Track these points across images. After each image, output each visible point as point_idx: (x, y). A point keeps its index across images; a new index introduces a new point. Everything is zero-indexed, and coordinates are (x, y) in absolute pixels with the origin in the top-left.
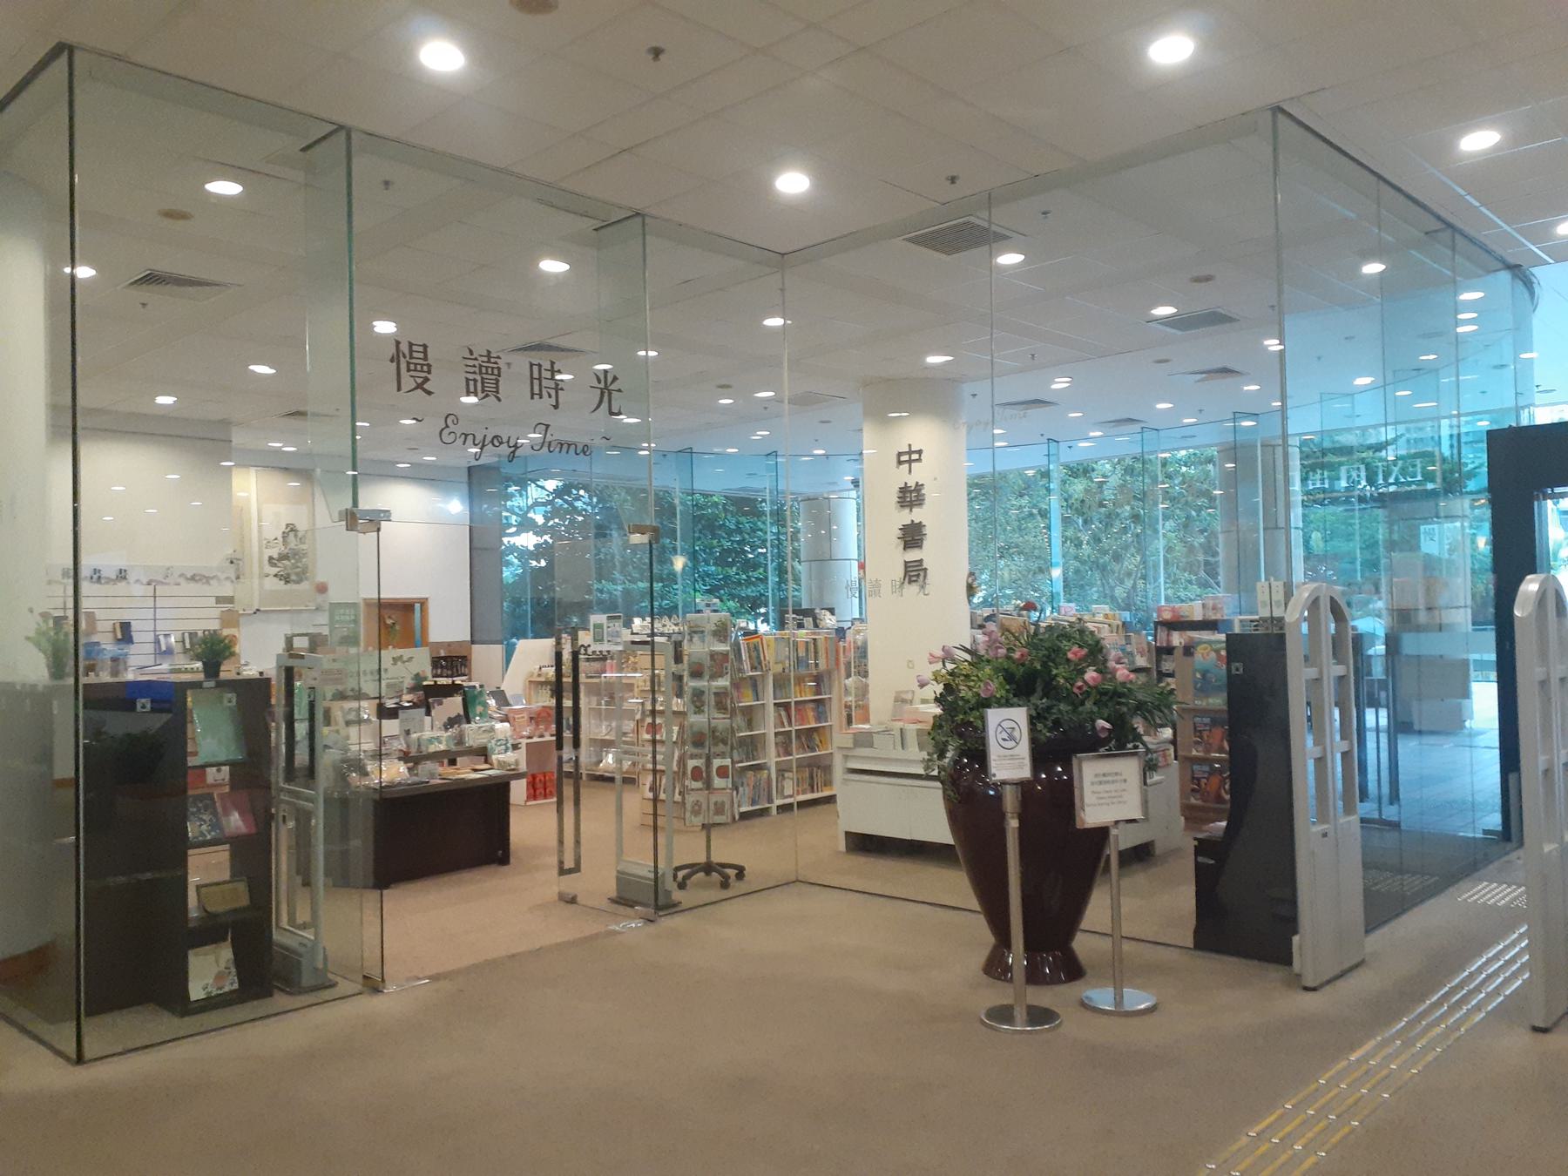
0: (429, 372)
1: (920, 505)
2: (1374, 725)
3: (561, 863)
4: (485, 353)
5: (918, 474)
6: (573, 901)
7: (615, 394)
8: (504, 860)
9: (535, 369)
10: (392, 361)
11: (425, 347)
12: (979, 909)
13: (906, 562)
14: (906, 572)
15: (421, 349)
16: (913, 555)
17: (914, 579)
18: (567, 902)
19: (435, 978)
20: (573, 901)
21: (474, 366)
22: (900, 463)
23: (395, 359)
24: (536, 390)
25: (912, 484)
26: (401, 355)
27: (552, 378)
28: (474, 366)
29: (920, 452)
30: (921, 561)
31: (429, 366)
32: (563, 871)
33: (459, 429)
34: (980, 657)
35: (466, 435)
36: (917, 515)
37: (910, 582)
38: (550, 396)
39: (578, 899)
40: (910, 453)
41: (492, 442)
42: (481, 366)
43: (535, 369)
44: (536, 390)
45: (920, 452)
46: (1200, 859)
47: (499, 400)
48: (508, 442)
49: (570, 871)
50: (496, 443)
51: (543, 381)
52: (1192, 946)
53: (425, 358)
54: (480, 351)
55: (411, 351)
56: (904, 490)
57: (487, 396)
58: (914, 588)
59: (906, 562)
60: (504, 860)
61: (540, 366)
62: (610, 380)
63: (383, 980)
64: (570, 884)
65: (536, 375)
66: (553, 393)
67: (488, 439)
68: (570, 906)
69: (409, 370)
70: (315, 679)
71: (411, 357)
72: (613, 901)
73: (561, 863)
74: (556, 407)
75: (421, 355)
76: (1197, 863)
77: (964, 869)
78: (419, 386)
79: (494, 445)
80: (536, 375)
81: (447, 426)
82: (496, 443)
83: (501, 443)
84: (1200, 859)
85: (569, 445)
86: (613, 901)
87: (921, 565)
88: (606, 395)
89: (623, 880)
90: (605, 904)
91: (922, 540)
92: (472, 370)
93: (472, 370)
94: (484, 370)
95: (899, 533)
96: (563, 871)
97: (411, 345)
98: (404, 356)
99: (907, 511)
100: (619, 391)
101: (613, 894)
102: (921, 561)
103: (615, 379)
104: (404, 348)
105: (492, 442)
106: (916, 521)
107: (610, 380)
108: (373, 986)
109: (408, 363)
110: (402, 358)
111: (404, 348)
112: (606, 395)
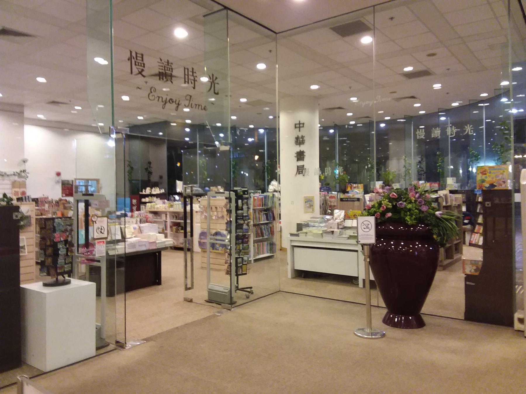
0: (144, 67)
1: (303, 144)
2: (114, 232)
3: (186, 285)
4: (167, 61)
5: (303, 132)
6: (191, 301)
7: (216, 85)
8: (159, 283)
9: (186, 70)
10: (129, 60)
11: (142, 55)
12: (385, 307)
13: (298, 166)
14: (298, 169)
15: (141, 56)
16: (300, 163)
17: (301, 172)
18: (189, 302)
19: (147, 340)
20: (191, 301)
21: (162, 66)
22: (296, 127)
23: (130, 59)
24: (187, 80)
25: (300, 136)
26: (132, 57)
27: (193, 75)
28: (162, 66)
29: (303, 124)
30: (303, 166)
31: (144, 64)
32: (187, 289)
33: (156, 95)
34: (202, 212)
35: (159, 97)
36: (302, 148)
37: (299, 173)
38: (192, 83)
39: (193, 300)
40: (300, 124)
41: (169, 101)
42: (165, 67)
43: (186, 70)
44: (187, 80)
45: (303, 124)
46: (468, 283)
47: (172, 82)
48: (176, 102)
49: (190, 289)
50: (171, 101)
51: (189, 76)
52: (463, 318)
53: (142, 60)
54: (165, 59)
55: (136, 56)
56: (297, 138)
57: (167, 80)
58: (301, 175)
59: (298, 166)
60: (159, 283)
61: (188, 69)
62: (214, 78)
63: (126, 343)
64: (190, 294)
65: (186, 73)
66: (193, 82)
67: (168, 99)
68: (190, 303)
69: (136, 65)
70: (96, 205)
71: (137, 59)
72: (207, 301)
73: (186, 285)
74: (194, 88)
75: (141, 59)
76: (466, 284)
77: (378, 288)
78: (140, 73)
79: (170, 103)
80: (186, 73)
81: (151, 92)
82: (171, 101)
83: (173, 102)
84: (468, 283)
85: (199, 105)
86: (207, 301)
87: (303, 167)
88: (213, 84)
89: (211, 292)
90: (203, 302)
91: (304, 158)
92: (161, 68)
93: (161, 68)
94: (166, 69)
95: (296, 155)
96: (187, 289)
97: (136, 53)
98: (134, 58)
99: (298, 146)
100: (218, 84)
101: (207, 298)
102: (303, 166)
103: (216, 78)
104: (134, 55)
105: (169, 101)
106: (302, 150)
107: (214, 78)
108: (120, 345)
109: (135, 62)
110: (133, 60)
111: (134, 55)
112: (213, 84)
